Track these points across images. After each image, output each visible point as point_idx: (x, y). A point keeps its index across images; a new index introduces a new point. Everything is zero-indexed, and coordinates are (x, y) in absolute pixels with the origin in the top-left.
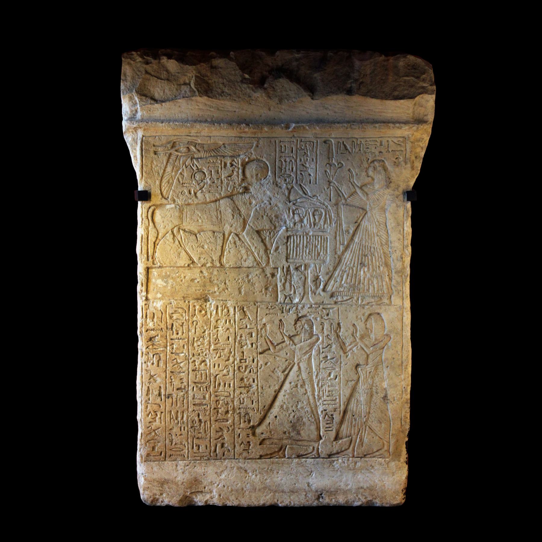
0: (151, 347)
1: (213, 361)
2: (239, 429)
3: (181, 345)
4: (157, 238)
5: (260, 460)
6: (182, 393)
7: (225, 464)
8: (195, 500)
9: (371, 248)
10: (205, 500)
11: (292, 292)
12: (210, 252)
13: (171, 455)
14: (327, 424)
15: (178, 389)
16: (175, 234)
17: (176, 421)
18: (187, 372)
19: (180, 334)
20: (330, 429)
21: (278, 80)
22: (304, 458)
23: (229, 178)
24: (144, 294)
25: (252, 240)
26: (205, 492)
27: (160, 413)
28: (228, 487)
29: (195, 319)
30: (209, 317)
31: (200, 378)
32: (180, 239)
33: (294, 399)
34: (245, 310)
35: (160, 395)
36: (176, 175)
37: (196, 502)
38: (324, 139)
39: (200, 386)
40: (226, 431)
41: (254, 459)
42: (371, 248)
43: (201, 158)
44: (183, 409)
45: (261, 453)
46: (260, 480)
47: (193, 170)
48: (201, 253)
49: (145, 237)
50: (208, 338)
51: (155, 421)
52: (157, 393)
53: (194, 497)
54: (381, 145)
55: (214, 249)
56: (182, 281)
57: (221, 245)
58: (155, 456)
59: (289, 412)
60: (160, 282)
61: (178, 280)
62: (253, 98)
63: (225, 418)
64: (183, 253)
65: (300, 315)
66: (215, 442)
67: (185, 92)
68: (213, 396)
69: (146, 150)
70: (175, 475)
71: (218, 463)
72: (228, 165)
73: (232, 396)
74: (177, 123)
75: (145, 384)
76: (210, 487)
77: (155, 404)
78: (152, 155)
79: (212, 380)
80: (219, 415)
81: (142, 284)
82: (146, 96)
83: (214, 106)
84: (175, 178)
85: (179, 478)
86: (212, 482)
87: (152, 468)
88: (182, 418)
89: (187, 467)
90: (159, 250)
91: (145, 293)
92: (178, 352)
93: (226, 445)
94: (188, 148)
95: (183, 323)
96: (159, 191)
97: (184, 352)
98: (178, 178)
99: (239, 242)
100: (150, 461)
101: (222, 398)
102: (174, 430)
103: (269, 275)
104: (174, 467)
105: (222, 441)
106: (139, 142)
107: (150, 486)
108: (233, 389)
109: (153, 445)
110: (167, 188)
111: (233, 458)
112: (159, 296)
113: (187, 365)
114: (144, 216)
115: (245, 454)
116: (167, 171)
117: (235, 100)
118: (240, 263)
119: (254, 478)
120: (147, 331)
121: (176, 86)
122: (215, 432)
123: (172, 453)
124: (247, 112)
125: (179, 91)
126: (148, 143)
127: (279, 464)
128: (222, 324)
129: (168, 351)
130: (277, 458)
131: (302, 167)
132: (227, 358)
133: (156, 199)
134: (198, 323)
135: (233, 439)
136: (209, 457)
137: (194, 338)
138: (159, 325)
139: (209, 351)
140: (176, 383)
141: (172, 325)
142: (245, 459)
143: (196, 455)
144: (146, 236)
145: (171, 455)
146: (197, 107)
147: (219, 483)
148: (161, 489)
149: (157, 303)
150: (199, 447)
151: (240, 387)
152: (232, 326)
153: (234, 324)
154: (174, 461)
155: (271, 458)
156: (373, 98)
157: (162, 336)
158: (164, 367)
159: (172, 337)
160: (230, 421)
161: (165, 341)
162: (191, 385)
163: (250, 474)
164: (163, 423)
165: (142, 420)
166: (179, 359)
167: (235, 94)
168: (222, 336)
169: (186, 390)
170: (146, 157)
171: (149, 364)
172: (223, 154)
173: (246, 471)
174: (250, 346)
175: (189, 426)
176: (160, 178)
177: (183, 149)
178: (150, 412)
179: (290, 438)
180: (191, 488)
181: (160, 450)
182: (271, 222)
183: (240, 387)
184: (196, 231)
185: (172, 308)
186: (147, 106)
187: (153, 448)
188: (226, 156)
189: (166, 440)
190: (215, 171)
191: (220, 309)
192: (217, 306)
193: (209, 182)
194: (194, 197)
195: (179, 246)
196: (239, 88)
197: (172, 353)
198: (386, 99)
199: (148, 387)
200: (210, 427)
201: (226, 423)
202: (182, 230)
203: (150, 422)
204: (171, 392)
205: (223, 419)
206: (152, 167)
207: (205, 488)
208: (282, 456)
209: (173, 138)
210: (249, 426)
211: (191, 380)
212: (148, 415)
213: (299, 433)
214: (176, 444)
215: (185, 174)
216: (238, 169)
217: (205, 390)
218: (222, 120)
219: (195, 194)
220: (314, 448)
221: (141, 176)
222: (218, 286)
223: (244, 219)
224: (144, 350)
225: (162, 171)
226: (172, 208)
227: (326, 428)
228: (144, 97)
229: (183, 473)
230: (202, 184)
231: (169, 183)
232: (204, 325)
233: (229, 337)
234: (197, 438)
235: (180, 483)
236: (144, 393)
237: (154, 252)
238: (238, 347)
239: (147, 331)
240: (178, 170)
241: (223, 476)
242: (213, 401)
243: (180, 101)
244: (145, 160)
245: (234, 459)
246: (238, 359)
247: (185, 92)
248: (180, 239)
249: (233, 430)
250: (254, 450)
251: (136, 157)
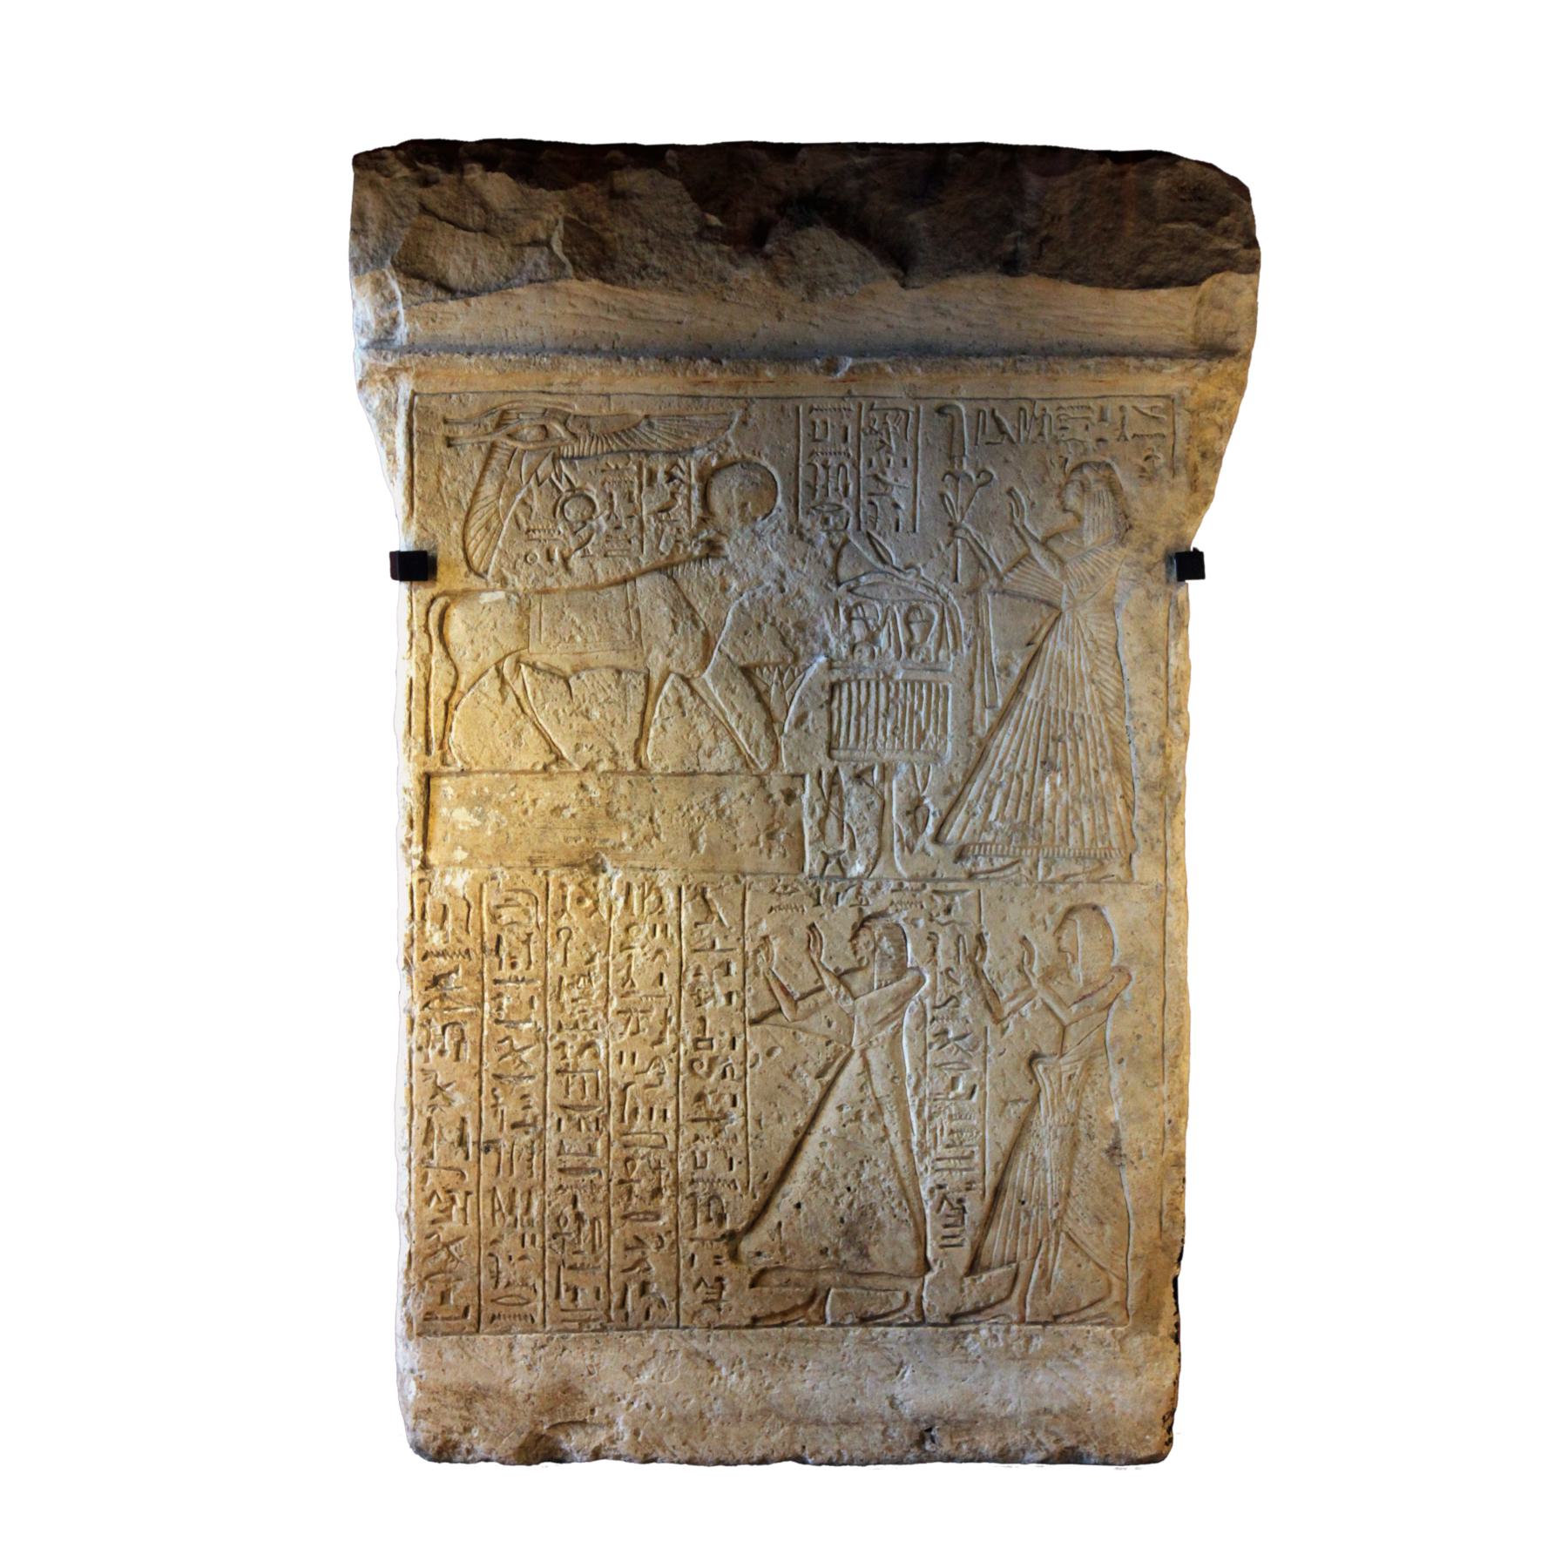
0: (436, 1003)
1: (618, 1046)
2: (692, 1240)
3: (525, 998)
4: (454, 688)
5: (751, 1331)
6: (527, 1138)
7: (652, 1341)
9: (1072, 716)
11: (845, 846)
12: (609, 728)
13: (493, 1318)
14: (946, 1226)
15: (514, 1126)
16: (507, 677)
17: (509, 1219)
18: (540, 1075)
19: (521, 965)
20: (954, 1241)
21: (804, 233)
22: (879, 1325)
23: (664, 516)
25: (728, 694)
26: (592, 1424)
27: (462, 1194)
28: (660, 1409)
29: (563, 922)
30: (605, 916)
31: (580, 1094)
32: (520, 693)
33: (850, 1155)
34: (709, 896)
35: (462, 1141)
36: (509, 507)
38: (936, 403)
39: (577, 1115)
40: (653, 1247)
41: (734, 1327)
42: (1072, 716)
43: (581, 458)
44: (528, 1182)
45: (755, 1311)
46: (752, 1388)
47: (559, 491)
48: (583, 733)
49: (419, 684)
50: (602, 979)
51: (450, 1217)
52: (455, 1136)
53: (562, 1437)
54: (1102, 419)
55: (619, 721)
56: (526, 812)
57: (640, 709)
58: (449, 1319)
59: (837, 1192)
60: (462, 816)
61: (516, 809)
62: (732, 284)
63: (651, 1208)
64: (530, 733)
65: (868, 911)
66: (622, 1277)
67: (536, 265)
68: (615, 1146)
69: (423, 433)
70: (507, 1374)
71: (630, 1339)
72: (661, 476)
73: (671, 1147)
74: (512, 357)
75: (420, 1112)
76: (608, 1409)
77: (450, 1168)
78: (440, 447)
79: (613, 1099)
80: (634, 1200)
81: (411, 821)
82: (421, 277)
83: (618, 306)
84: (506, 515)
85: (518, 1384)
86: (612, 1394)
87: (440, 1355)
88: (528, 1209)
89: (542, 1352)
90: (459, 722)
91: (420, 849)
92: (514, 1017)
93: (654, 1288)
94: (544, 427)
95: (529, 935)
96: (461, 553)
97: (533, 1017)
98: (515, 516)
99: (691, 699)
100: (435, 1333)
101: (643, 1151)
102: (504, 1245)
103: (777, 796)
104: (505, 1350)
105: (642, 1277)
106: (402, 411)
107: (433, 1405)
108: (674, 1125)
109: (442, 1287)
110: (483, 545)
111: (674, 1324)
112: (460, 855)
113: (541, 1057)
115: (708, 1314)
116: (482, 496)
117: (680, 290)
118: (694, 760)
120: (424, 958)
121: (509, 249)
122: (621, 1250)
123: (497, 1309)
124: (715, 325)
125: (519, 264)
126: (427, 414)
127: (808, 1341)
128: (642, 937)
129: (486, 1016)
130: (800, 1325)
131: (873, 482)
132: (655, 1036)
133: (450, 577)
134: (574, 935)
135: (673, 1269)
136: (604, 1321)
137: (561, 979)
138: (459, 941)
139: (606, 1015)
140: (511, 1108)
141: (499, 939)
142: (709, 1327)
143: (568, 1315)
144: (423, 684)
145: (493, 1318)
146: (569, 310)
147: (635, 1397)
148: (465, 1414)
149: (454, 877)
150: (576, 1294)
151: (694, 1121)
152: (672, 942)
153: (676, 939)
154: (502, 1333)
155: (783, 1325)
156: (1078, 283)
157: (468, 973)
158: (476, 1062)
159: (498, 975)
160: (665, 1219)
161: (477, 987)
162: (554, 1114)
163: (724, 1372)
164: (471, 1224)
165: (412, 1215)
166: (519, 1038)
167: (680, 271)
168: (641, 971)
169: (540, 1127)
170: (422, 453)
171: (432, 1053)
172: (644, 447)
173: (711, 1362)
174: (723, 1001)
175: (547, 1232)
176: (462, 516)
177: (530, 432)
178: (434, 1192)
179: (838, 1266)
180: (551, 1410)
181: (462, 1303)
182: (784, 643)
183: (694, 1121)
184: (568, 669)
185: (498, 890)
186: (425, 305)
187: (444, 1297)
188: (653, 452)
189: (479, 1273)
190: (622, 496)
191: (635, 893)
192: (629, 886)
193: (605, 527)
194: (561, 570)
195: (519, 711)
196: (690, 255)
197: (497, 1021)
198: (1118, 287)
199: (429, 1120)
200: (608, 1237)
201: (654, 1224)
202: (527, 665)
203: (433, 1222)
204: (495, 1134)
205: (646, 1212)
206: (439, 482)
207: (593, 1411)
208: (815, 1318)
209: (499, 400)
210: (722, 1231)
211: (552, 1098)
212: (428, 1201)
213: (864, 1253)
214: (508, 1284)
215: (536, 505)
216: (690, 488)
217: (593, 1127)
218: (643, 346)
219: (565, 560)
220: (907, 1296)
221: (407, 508)
222: (631, 827)
223: (706, 634)
225: (469, 495)
226: (497, 602)
227: (944, 1237)
228: (418, 282)
229: (530, 1367)
230: (584, 533)
231: (488, 529)
232: (590, 940)
233: (661, 975)
234: (571, 1268)
235: (520, 1398)
237: (447, 728)
238: (688, 1004)
239: (424, 958)
240: (514, 493)
241: (645, 1378)
242: (616, 1159)
243: (519, 291)
244: (420, 462)
245: (678, 1327)
246: (689, 1038)
247: (536, 265)
248: (520, 693)
249: (675, 1243)
250: (733, 1302)
251: (395, 455)
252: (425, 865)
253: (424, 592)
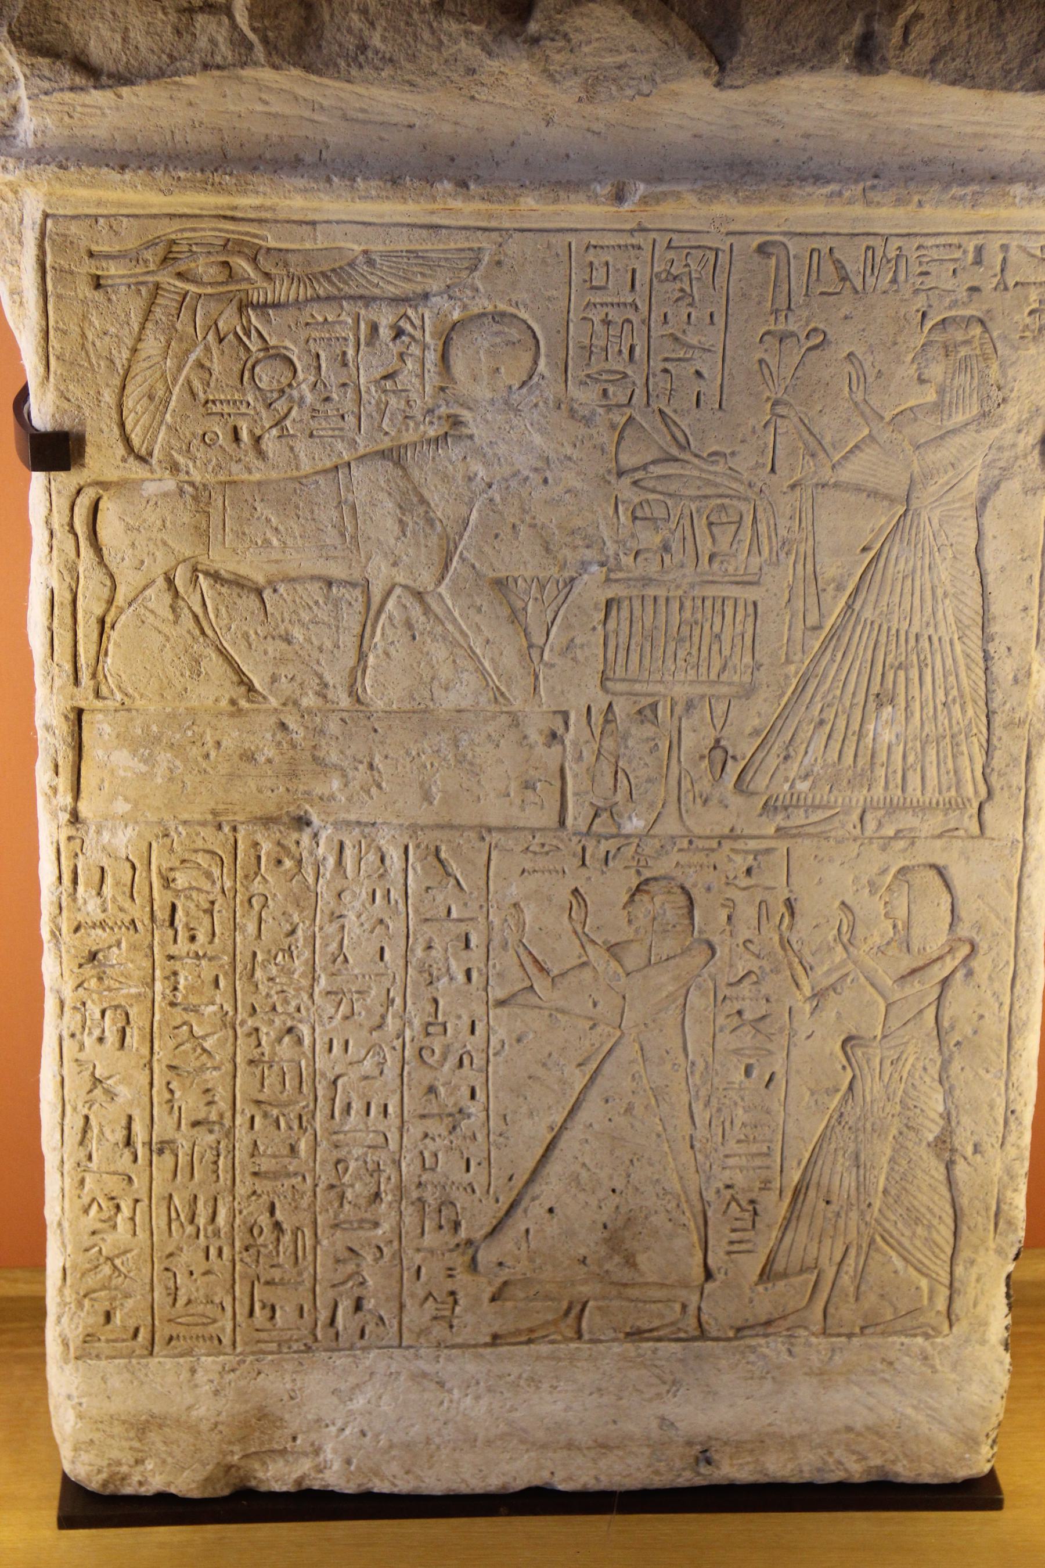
0: (93, 983)
1: (326, 1032)
2: (418, 1250)
3: (208, 975)
4: (111, 602)
5: (489, 1350)
6: (211, 1138)
7: (368, 1363)
8: (260, 1475)
9: (917, 637)
10: (295, 1476)
11: (620, 797)
12: (315, 654)
13: (171, 1339)
14: (734, 1230)
15: (196, 1124)
16: (181, 590)
17: (190, 1229)
18: (229, 1066)
19: (201, 938)
20: (743, 1247)
21: (584, 10)
22: (648, 1340)
23: (389, 385)
24: (65, 799)
25: (472, 612)
26: (292, 1453)
27: (130, 1203)
28: (377, 1436)
29: (257, 886)
30: (311, 880)
31: (279, 1087)
32: (198, 610)
33: (617, 1153)
34: (443, 855)
35: (128, 1142)
36: (180, 369)
37: (261, 1481)
38: (759, 240)
39: (275, 1112)
40: (369, 1259)
41: (469, 1346)
42: (917, 637)
43: (276, 305)
44: (213, 1189)
45: (496, 1329)
46: (490, 1411)
47: (247, 349)
48: (281, 660)
49: (63, 596)
50: (307, 954)
51: (114, 1227)
52: (120, 1135)
53: (257, 1466)
54: (978, 262)
55: (328, 644)
56: (207, 756)
57: (357, 630)
58: (115, 1341)
59: (601, 1194)
60: (122, 758)
61: (194, 752)
62: (484, 78)
63: (368, 1216)
64: (213, 663)
65: (647, 874)
66: (331, 1294)
67: (213, 41)
68: (324, 1145)
69: (58, 270)
70: (189, 1400)
71: (341, 1360)
72: (385, 333)
73: (393, 1145)
74: (182, 174)
75: (75, 1109)
76: (313, 1436)
77: (114, 1173)
78: (84, 289)
79: (320, 1094)
80: (347, 1207)
81: (56, 766)
82: (52, 53)
83: (326, 103)
84: (175, 380)
85: (201, 1411)
86: (318, 1420)
87: (104, 1379)
88: (213, 1218)
89: (232, 1375)
90: (117, 645)
91: (69, 799)
92: (194, 1000)
93: (369, 1304)
94: (226, 264)
95: (213, 903)
96: (116, 431)
97: (218, 1001)
98: (189, 382)
99: (422, 619)
100: (98, 1357)
101: (357, 1152)
102: (184, 1258)
103: (534, 736)
104: (185, 1375)
105: (357, 1292)
106: (30, 237)
107: (96, 1436)
108: (397, 1122)
109: (106, 1305)
110: (145, 419)
111: (396, 1343)
112: (121, 807)
113: (229, 1044)
114: (58, 521)
115: (439, 1331)
116: (143, 355)
117: (411, 84)
118: (427, 694)
119: (475, 1409)
120: (77, 929)
121: (173, 17)
122: (330, 1262)
123: (174, 1330)
124: (460, 130)
125: (188, 38)
126: (65, 244)
127: (560, 1359)
128: (357, 904)
129: (158, 998)
130: (552, 1342)
131: (668, 344)
132: (376, 1020)
133: (102, 459)
134: (270, 902)
135: (395, 1285)
136: (309, 1341)
137: (255, 954)
138: (121, 909)
139: (311, 996)
140: (190, 1103)
141: (174, 907)
142: (438, 1345)
143: (263, 1335)
144: (69, 597)
145: (171, 1339)
146: (260, 108)
147: (346, 1424)
148: (136, 1444)
149: (114, 834)
150: (273, 1309)
151: (423, 1117)
152: (397, 912)
153: (401, 906)
154: (181, 1356)
155: (530, 1341)
156: (954, 83)
157: (134, 947)
158: (146, 1051)
159: (173, 950)
160: (385, 1227)
161: (146, 964)
162: (245, 1109)
163: (456, 1394)
164: (142, 1235)
165: (66, 1224)
166: (200, 1024)
167: (413, 58)
168: (356, 945)
169: (227, 1123)
170: (59, 297)
171: (89, 1041)
172: (361, 291)
173: (441, 1384)
174: (461, 978)
175: (237, 1244)
176: (117, 382)
177: (204, 267)
178: (94, 1200)
179: (604, 1277)
180: (243, 1440)
181: (132, 1324)
182: (547, 550)
183: (423, 1117)
184: (260, 579)
185: (172, 850)
186: (58, 96)
187: (108, 1317)
188: (374, 299)
189: (152, 1290)
190: (332, 359)
191: (349, 853)
192: (342, 845)
193: (309, 398)
194: (252, 454)
195: (197, 632)
196: (426, 35)
197: (173, 1004)
198: (1008, 88)
199: (87, 1118)
200: (315, 1248)
201: (372, 1233)
202: (207, 574)
203: (94, 1233)
204: (170, 1134)
205: (362, 1221)
206: (83, 335)
207: (294, 1439)
208: (570, 1333)
209: (169, 229)
210: (456, 1241)
211: (243, 1093)
212: (86, 1211)
213: (630, 1262)
214: (189, 1302)
215: (216, 367)
216: (425, 347)
217: (295, 1125)
218: (361, 158)
219: (258, 440)
220: (684, 1307)
221: (41, 370)
222: (344, 776)
223: (445, 537)
224: (68, 994)
225: (126, 354)
226: (165, 495)
227: (732, 1243)
228: (46, 61)
229: (216, 1393)
230: (281, 406)
231: (151, 398)
232: (290, 909)
233: (382, 949)
234: (267, 1283)
235: (204, 1427)
236: (72, 1136)
237: (101, 652)
238: (416, 983)
239: (77, 929)
240: (187, 352)
241: (360, 1402)
242: (324, 1162)
243: (190, 80)
244: (57, 309)
245: (400, 1346)
246: (416, 1022)
247: (213, 41)
248: (198, 610)
249: (398, 1255)
250: (469, 1318)
251: (20, 294)
252: (75, 818)
253: (65, 481)
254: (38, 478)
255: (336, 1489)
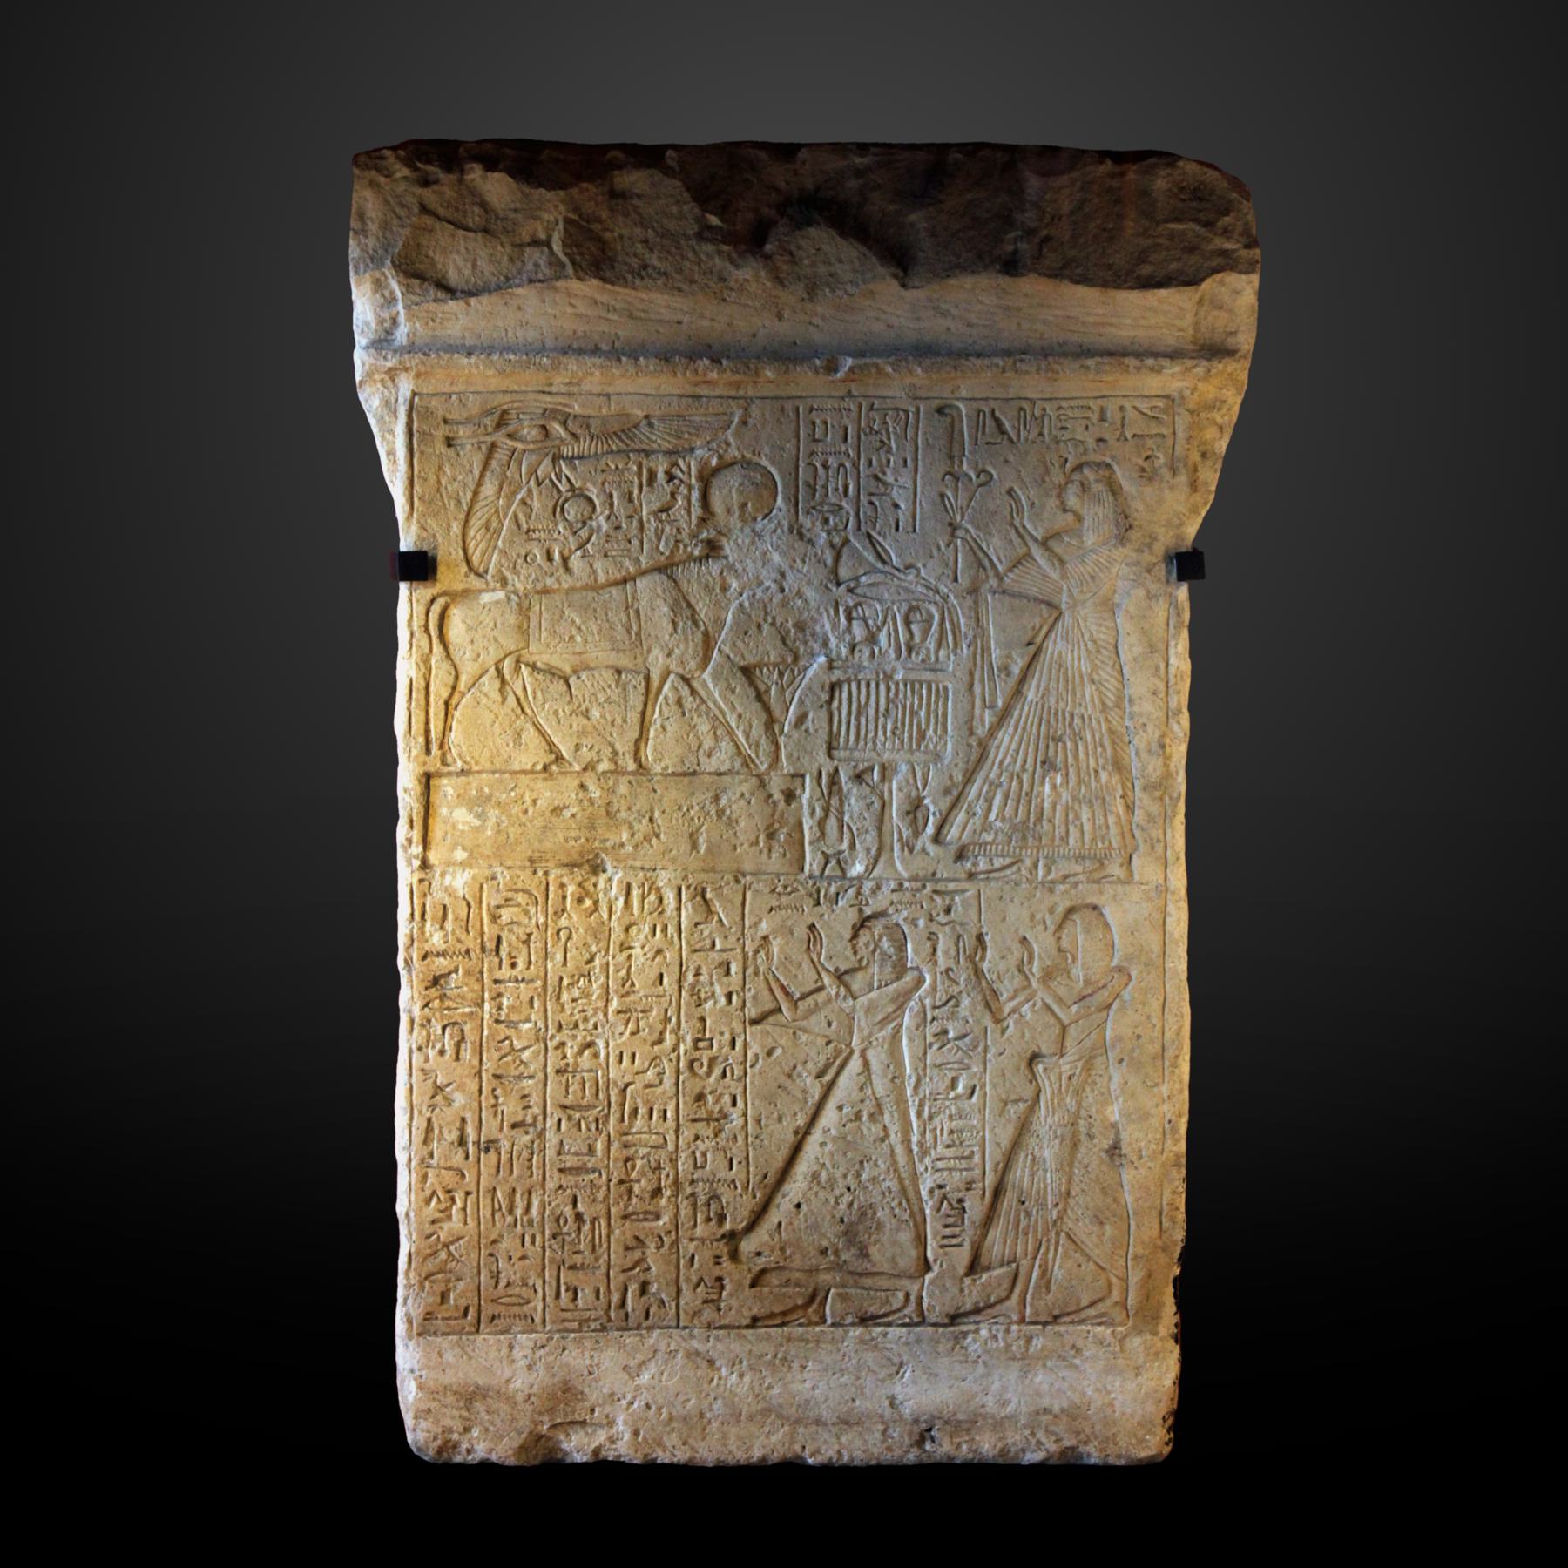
0: (436, 1003)
1: (618, 1046)
2: (692, 1240)
3: (525, 998)
4: (454, 688)
5: (751, 1331)
6: (527, 1138)
7: (652, 1341)
8: (565, 1446)
9: (1072, 716)
10: (593, 1446)
11: (845, 846)
12: (609, 728)
13: (493, 1318)
14: (946, 1226)
15: (514, 1126)
16: (507, 677)
17: (509, 1219)
18: (540, 1075)
19: (521, 965)
20: (954, 1241)
21: (804, 233)
22: (879, 1325)
23: (664, 516)
24: (417, 849)
25: (728, 694)
26: (592, 1424)
27: (462, 1194)
28: (660, 1409)
29: (563, 922)
30: (605, 916)
31: (580, 1094)
32: (520, 693)
33: (850, 1155)
34: (709, 896)
35: (462, 1141)
36: (509, 507)
37: (566, 1454)
38: (936, 403)
39: (577, 1115)
40: (653, 1247)
41: (734, 1327)
42: (1072, 716)
43: (581, 458)
44: (528, 1182)
45: (755, 1311)
46: (752, 1388)
47: (559, 491)
48: (583, 733)
49: (419, 684)
50: (602, 979)
51: (450, 1217)
52: (455, 1136)
53: (562, 1437)
54: (1102, 419)
55: (619, 721)
56: (526, 812)
57: (640, 709)
58: (449, 1319)
59: (837, 1192)
60: (462, 816)
61: (516, 809)
62: (732, 284)
63: (651, 1208)
64: (530, 733)
65: (868, 911)
66: (622, 1277)
67: (536, 265)
68: (615, 1146)
69: (423, 433)
70: (507, 1374)
71: (630, 1339)
72: (661, 476)
73: (671, 1147)
74: (512, 357)
75: (420, 1112)
76: (608, 1409)
77: (450, 1168)
78: (440, 447)
79: (613, 1099)
80: (634, 1200)
81: (411, 821)
82: (421, 277)
83: (618, 306)
84: (506, 515)
85: (518, 1384)
86: (612, 1394)
87: (440, 1355)
88: (528, 1209)
89: (542, 1352)
90: (459, 722)
91: (420, 849)
92: (514, 1017)
93: (654, 1288)
94: (544, 427)
95: (529, 935)
96: (461, 553)
97: (533, 1017)
98: (515, 516)
99: (691, 699)
100: (435, 1333)
101: (643, 1151)
102: (504, 1245)
103: (777, 796)
104: (505, 1350)
105: (642, 1277)
106: (402, 411)
107: (433, 1405)
108: (674, 1125)
109: (442, 1287)
110: (483, 545)
111: (674, 1324)
112: (460, 855)
113: (541, 1057)
114: (417, 624)
115: (708, 1314)
116: (482, 496)
117: (680, 290)
118: (694, 760)
119: (736, 1383)
120: (424, 958)
121: (509, 249)
122: (621, 1250)
123: (497, 1309)
124: (715, 325)
125: (519, 264)
126: (427, 414)
127: (808, 1341)
128: (642, 937)
129: (486, 1016)
130: (800, 1325)
131: (873, 482)
132: (655, 1036)
133: (450, 577)
134: (574, 935)
135: (673, 1269)
136: (604, 1321)
137: (561, 979)
138: (459, 941)
139: (606, 1015)
140: (511, 1108)
141: (499, 939)
142: (709, 1327)
143: (568, 1315)
144: (423, 684)
145: (493, 1318)
146: (569, 310)
147: (635, 1397)
148: (465, 1414)
149: (454, 877)
150: (576, 1294)
151: (694, 1121)
152: (672, 942)
153: (676, 939)
154: (502, 1333)
155: (783, 1325)
156: (1078, 283)
157: (468, 973)
158: (476, 1062)
159: (498, 975)
160: (665, 1219)
161: (477, 987)
162: (554, 1114)
163: (724, 1372)
164: (471, 1224)
165: (412, 1215)
166: (519, 1038)
167: (680, 271)
168: (641, 971)
169: (540, 1127)
170: (422, 453)
171: (432, 1053)
172: (644, 447)
173: (711, 1362)
174: (723, 1001)
175: (547, 1232)
176: (462, 516)
177: (530, 432)
178: (434, 1192)
179: (838, 1266)
180: (551, 1410)
181: (462, 1303)
182: (784, 643)
183: (694, 1121)
184: (568, 669)
185: (498, 890)
186: (425, 305)
187: (444, 1297)
188: (653, 452)
189: (479, 1273)
190: (622, 496)
191: (635, 893)
192: (629, 886)
193: (605, 527)
194: (561, 570)
195: (519, 711)
196: (690, 255)
197: (497, 1021)
198: (1118, 287)
199: (429, 1120)
200: (608, 1237)
201: (654, 1224)
202: (527, 665)
203: (433, 1222)
204: (495, 1134)
205: (646, 1212)
206: (439, 482)
207: (593, 1411)
208: (815, 1318)
209: (499, 400)
210: (722, 1231)
211: (552, 1098)
212: (428, 1201)
213: (864, 1253)
214: (508, 1284)
215: (536, 505)
216: (690, 488)
217: (593, 1127)
218: (643, 346)
219: (565, 560)
220: (907, 1296)
221: (407, 508)
222: (631, 827)
223: (706, 634)
224: (417, 1012)
225: (469, 495)
226: (497, 602)
227: (944, 1237)
228: (418, 282)
229: (530, 1367)
230: (584, 533)
231: (488, 529)
232: (590, 940)
233: (661, 975)
234: (571, 1268)
235: (520, 1398)
236: (418, 1137)
237: (447, 728)
238: (688, 1004)
239: (424, 958)
240: (514, 493)
241: (645, 1378)
242: (616, 1159)
243: (519, 291)
244: (420, 462)
245: (678, 1327)
246: (689, 1038)
247: (536, 265)
248: (520, 693)
249: (675, 1243)
250: (733, 1302)
251: (394, 455)
253: (424, 592)
254: (403, 587)
255: (627, 1460)
